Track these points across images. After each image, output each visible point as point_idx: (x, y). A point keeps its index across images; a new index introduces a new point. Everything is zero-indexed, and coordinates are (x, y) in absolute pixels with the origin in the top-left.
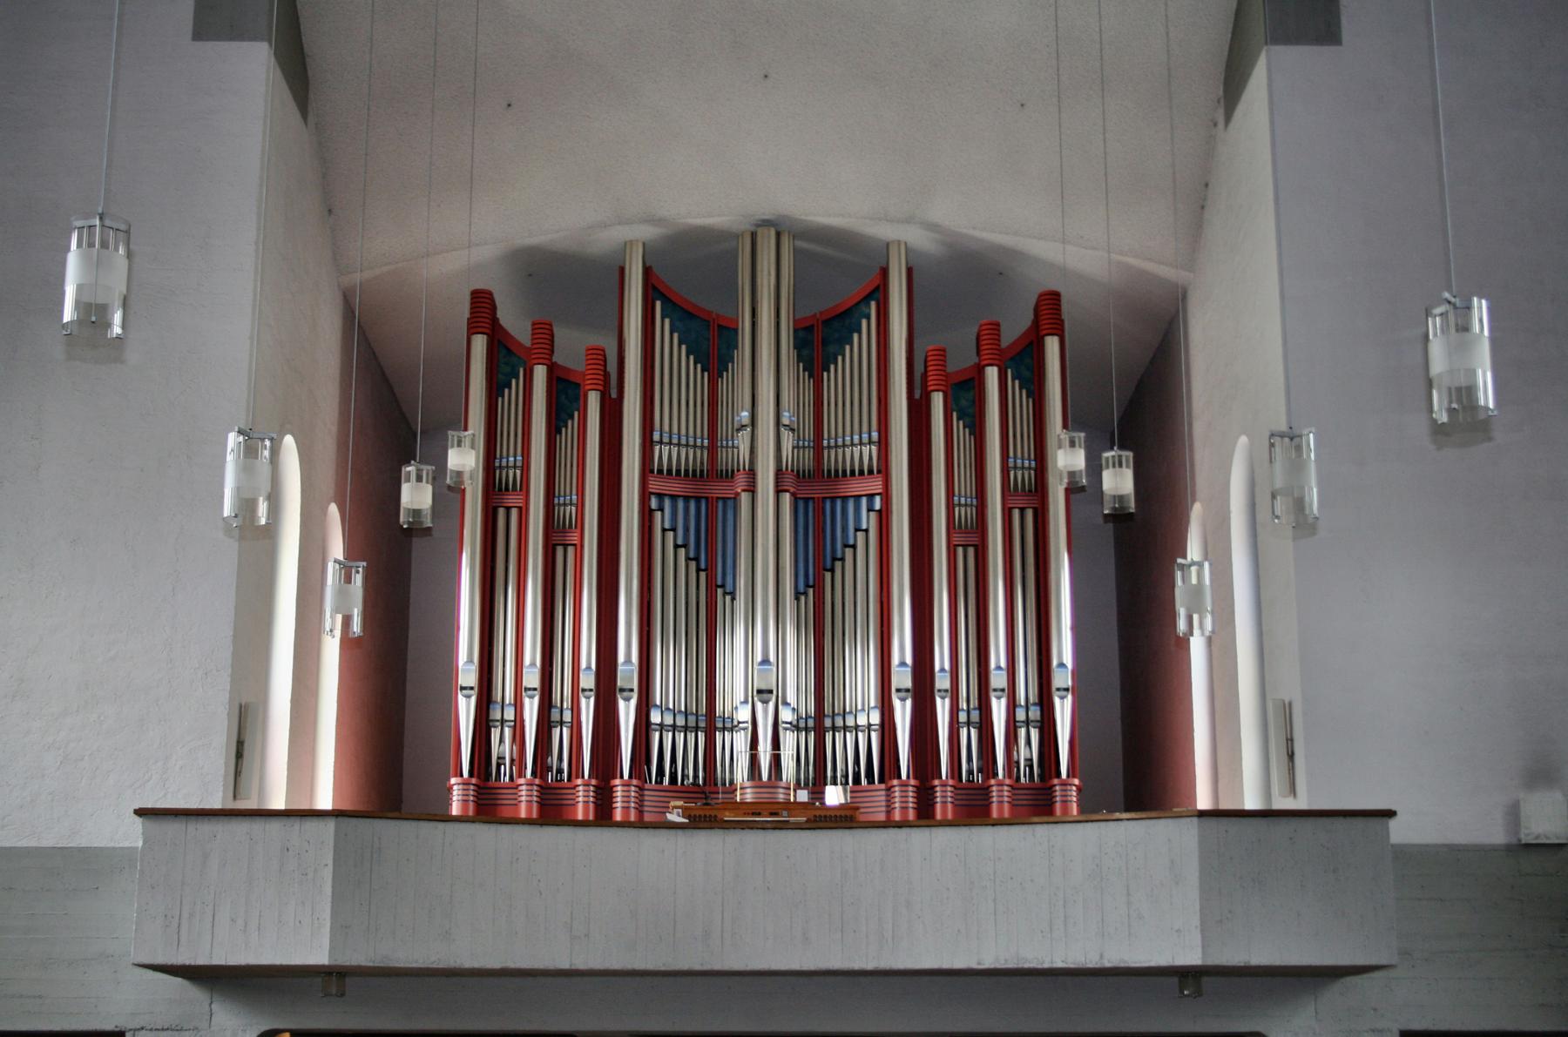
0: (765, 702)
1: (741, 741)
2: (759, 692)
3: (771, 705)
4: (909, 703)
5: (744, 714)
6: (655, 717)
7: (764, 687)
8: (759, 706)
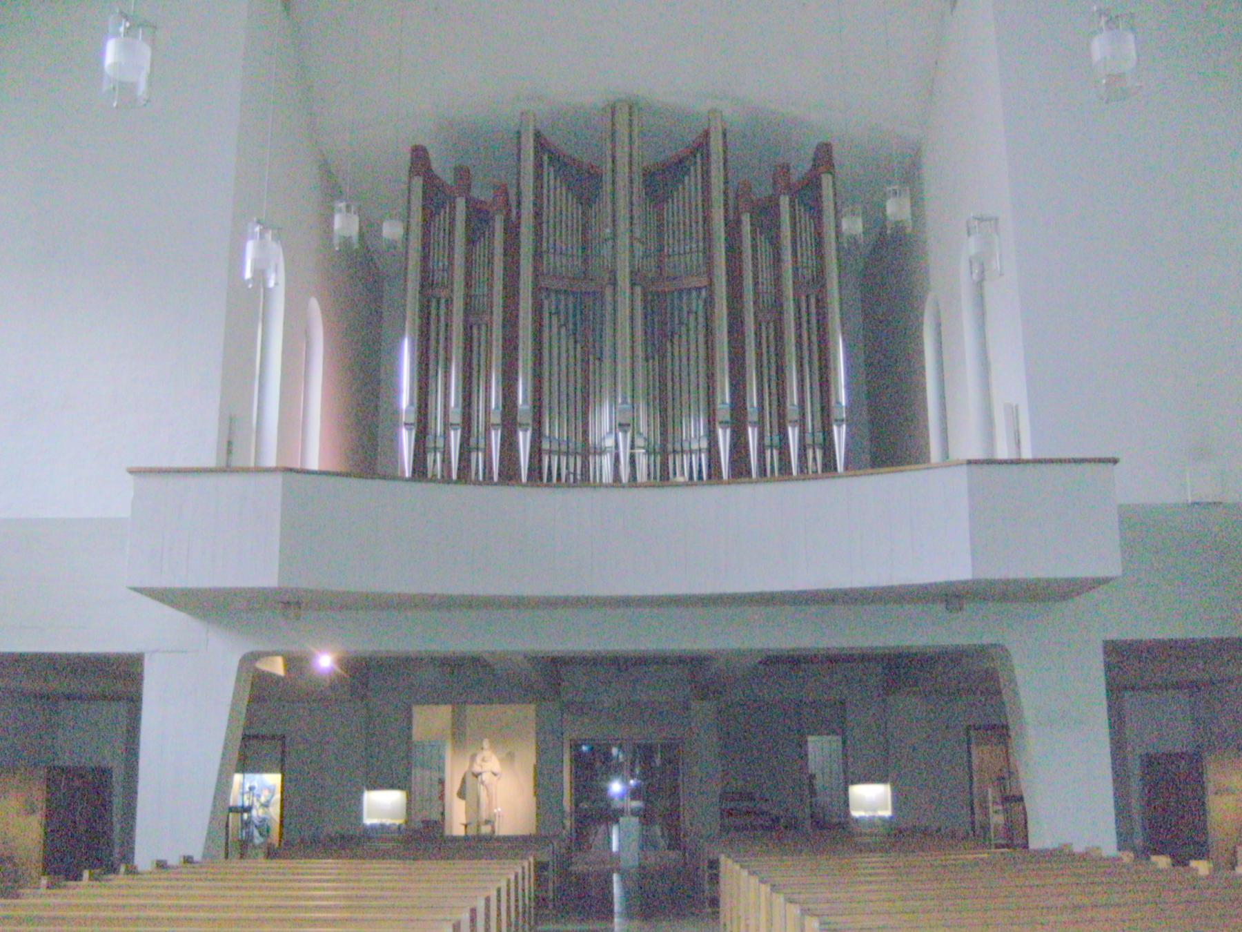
0: (625, 432)
1: (607, 461)
2: (621, 425)
3: (629, 435)
4: (728, 431)
5: (609, 442)
6: (546, 445)
7: (623, 421)
8: (620, 435)
